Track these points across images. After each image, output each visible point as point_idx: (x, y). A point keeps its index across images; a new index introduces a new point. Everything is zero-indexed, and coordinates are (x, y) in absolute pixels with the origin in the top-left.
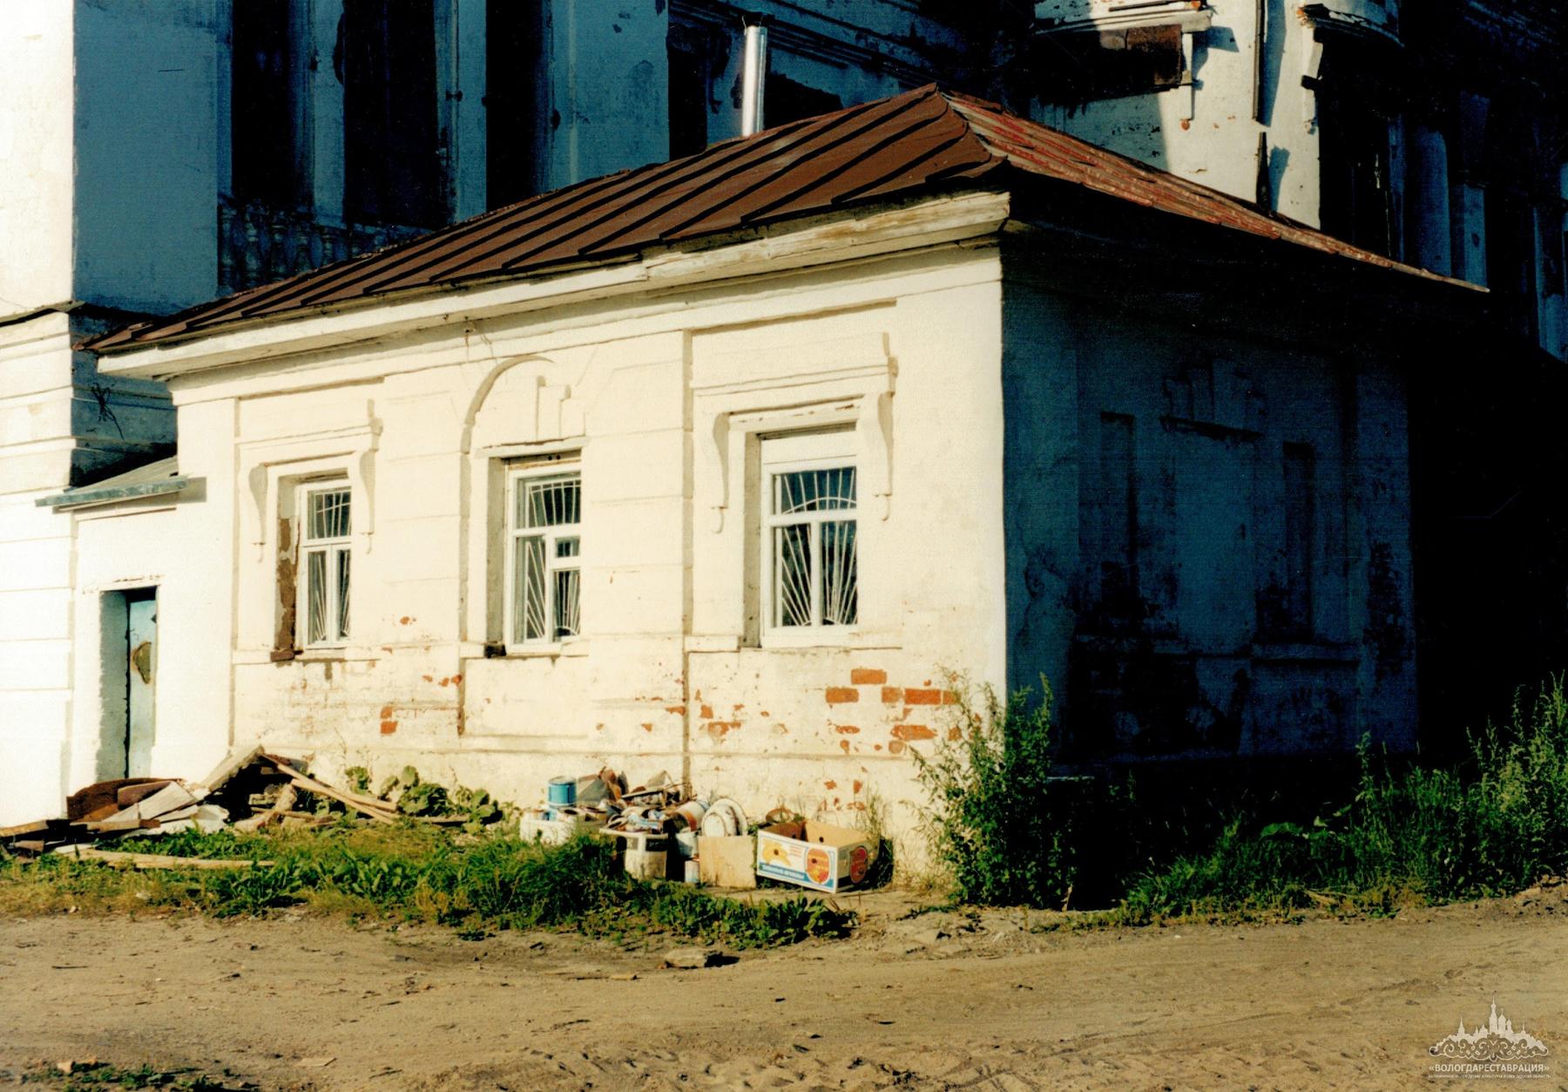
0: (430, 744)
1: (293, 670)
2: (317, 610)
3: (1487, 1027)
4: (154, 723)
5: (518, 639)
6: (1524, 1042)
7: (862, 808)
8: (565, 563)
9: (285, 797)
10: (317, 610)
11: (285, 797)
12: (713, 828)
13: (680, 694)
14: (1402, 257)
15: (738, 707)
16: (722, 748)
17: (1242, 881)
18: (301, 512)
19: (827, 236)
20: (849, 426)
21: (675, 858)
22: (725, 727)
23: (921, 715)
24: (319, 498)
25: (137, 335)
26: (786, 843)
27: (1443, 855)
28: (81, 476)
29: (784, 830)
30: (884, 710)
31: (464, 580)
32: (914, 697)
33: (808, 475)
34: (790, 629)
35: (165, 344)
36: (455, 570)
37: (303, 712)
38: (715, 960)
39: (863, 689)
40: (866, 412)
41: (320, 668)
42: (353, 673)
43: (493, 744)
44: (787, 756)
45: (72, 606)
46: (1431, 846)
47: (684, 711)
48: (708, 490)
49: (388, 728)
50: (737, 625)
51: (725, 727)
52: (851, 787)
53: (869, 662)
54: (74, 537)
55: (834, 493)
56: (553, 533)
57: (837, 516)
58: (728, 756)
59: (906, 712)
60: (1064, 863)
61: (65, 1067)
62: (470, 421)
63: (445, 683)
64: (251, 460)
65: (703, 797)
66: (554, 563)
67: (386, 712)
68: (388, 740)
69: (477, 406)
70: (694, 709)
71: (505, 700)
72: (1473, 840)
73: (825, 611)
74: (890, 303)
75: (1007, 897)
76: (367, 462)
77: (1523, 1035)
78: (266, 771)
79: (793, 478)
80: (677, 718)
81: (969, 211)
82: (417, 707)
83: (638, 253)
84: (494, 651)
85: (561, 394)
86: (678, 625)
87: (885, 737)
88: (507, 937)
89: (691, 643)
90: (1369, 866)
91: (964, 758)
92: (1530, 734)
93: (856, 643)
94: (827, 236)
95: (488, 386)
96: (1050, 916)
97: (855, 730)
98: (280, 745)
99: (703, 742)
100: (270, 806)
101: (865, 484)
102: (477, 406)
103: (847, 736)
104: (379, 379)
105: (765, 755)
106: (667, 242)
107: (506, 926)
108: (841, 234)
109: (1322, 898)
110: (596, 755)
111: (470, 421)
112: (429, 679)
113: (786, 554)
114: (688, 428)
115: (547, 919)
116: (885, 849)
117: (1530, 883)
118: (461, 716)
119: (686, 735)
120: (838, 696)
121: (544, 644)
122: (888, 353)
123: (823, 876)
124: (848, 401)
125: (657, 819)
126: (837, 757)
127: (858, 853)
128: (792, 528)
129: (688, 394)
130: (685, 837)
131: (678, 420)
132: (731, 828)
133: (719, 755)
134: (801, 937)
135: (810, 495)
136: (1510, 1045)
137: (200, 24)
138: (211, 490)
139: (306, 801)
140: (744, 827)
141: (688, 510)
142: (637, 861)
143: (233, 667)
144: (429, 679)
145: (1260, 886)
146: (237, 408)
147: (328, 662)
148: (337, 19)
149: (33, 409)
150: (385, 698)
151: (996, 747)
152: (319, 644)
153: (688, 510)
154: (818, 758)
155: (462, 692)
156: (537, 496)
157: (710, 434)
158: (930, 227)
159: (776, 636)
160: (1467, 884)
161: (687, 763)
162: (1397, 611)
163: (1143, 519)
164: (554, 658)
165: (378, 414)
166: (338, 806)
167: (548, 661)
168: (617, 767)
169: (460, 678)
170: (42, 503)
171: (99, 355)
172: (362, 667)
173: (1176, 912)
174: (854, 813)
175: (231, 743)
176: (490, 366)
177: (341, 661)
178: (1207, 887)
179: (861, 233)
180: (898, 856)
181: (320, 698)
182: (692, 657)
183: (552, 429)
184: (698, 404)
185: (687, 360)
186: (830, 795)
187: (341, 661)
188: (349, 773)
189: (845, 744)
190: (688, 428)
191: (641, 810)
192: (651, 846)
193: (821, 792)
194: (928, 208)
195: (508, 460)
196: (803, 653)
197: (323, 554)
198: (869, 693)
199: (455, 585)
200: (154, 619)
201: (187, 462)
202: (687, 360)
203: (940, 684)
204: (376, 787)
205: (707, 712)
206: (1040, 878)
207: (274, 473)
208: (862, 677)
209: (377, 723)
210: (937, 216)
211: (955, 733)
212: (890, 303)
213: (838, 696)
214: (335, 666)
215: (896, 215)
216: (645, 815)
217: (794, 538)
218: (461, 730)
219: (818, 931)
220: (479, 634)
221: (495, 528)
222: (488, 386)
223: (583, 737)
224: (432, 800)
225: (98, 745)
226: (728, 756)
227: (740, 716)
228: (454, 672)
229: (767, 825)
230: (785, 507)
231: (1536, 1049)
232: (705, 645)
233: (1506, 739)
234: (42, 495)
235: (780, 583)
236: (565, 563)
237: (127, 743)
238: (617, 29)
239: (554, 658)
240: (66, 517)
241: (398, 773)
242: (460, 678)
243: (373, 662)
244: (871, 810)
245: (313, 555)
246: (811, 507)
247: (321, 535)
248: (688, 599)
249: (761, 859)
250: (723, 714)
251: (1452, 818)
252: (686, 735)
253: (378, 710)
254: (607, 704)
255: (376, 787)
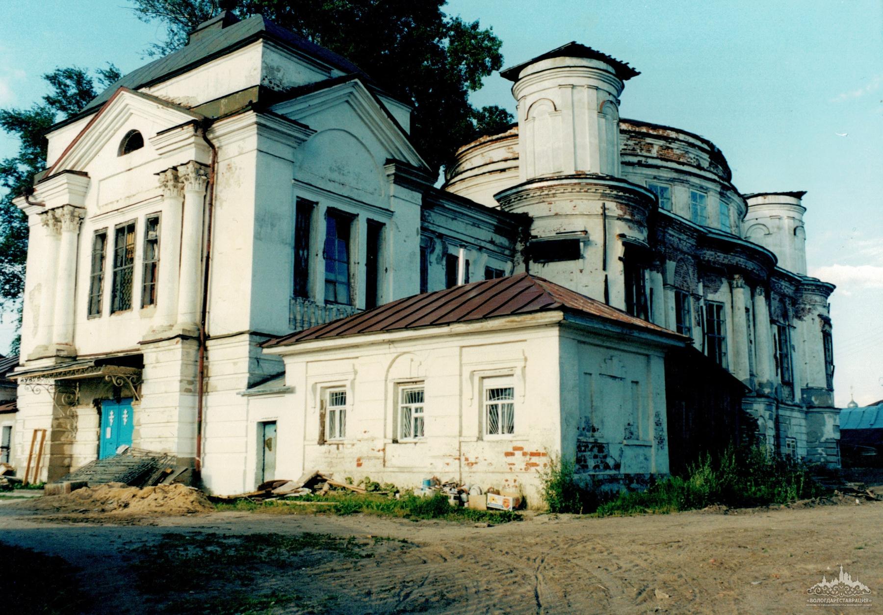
0: (373, 470)
1: (325, 448)
2: (332, 428)
3: (839, 580)
4: (275, 463)
5: (402, 438)
6: (858, 586)
7: (516, 487)
8: (419, 415)
9: (326, 487)
10: (332, 428)
11: (326, 487)
12: (473, 493)
13: (458, 454)
14: (635, 314)
15: (477, 458)
16: (471, 470)
17: (628, 506)
18: (328, 398)
19: (508, 322)
20: (512, 375)
21: (461, 503)
22: (472, 464)
23: (535, 460)
24: (333, 394)
25: (278, 343)
26: (496, 497)
27: (681, 499)
28: (251, 386)
29: (493, 492)
30: (523, 458)
31: (385, 419)
32: (532, 454)
33: (497, 390)
34: (491, 435)
35: (286, 345)
36: (383, 417)
37: (329, 460)
38: (489, 526)
39: (516, 452)
40: (518, 372)
41: (336, 446)
42: (346, 448)
43: (395, 470)
44: (493, 472)
45: (247, 427)
46: (678, 496)
47: (459, 459)
48: (467, 394)
49: (359, 465)
50: (477, 435)
51: (472, 464)
52: (513, 481)
53: (519, 444)
54: (248, 404)
55: (502, 395)
56: (414, 406)
57: (506, 402)
58: (474, 472)
59: (530, 459)
60: (580, 501)
61: (370, 536)
62: (388, 371)
63: (379, 451)
64: (311, 382)
65: (467, 484)
66: (414, 415)
67: (359, 460)
68: (359, 469)
69: (390, 366)
70: (463, 458)
71: (399, 456)
72: (689, 495)
73: (503, 430)
74: (525, 341)
75: (562, 511)
76: (353, 383)
77: (857, 583)
78: (319, 478)
79: (493, 391)
80: (457, 461)
81: (551, 317)
82: (369, 458)
83: (448, 324)
84: (395, 441)
85: (419, 364)
86: (458, 434)
87: (523, 466)
88: (425, 521)
89: (462, 439)
90: (661, 503)
91: (549, 471)
92: (704, 465)
93: (515, 439)
94: (508, 322)
95: (394, 361)
96: (577, 516)
97: (514, 464)
98: (324, 471)
99: (466, 468)
100: (321, 489)
101: (516, 393)
102: (390, 366)
103: (512, 466)
104: (357, 358)
105: (486, 472)
106: (458, 321)
107: (423, 518)
108: (512, 321)
109: (650, 511)
110: (430, 473)
111: (388, 371)
112: (373, 450)
113: (491, 413)
114: (461, 375)
115: (434, 517)
116: (524, 499)
117: (705, 507)
118: (384, 461)
119: (460, 466)
120: (508, 454)
121: (411, 439)
122: (524, 355)
123: (508, 506)
124: (512, 368)
125: (455, 491)
126: (508, 473)
127: (517, 500)
128: (492, 406)
129: (461, 365)
130: (464, 496)
131: (458, 373)
132: (479, 493)
133: (471, 472)
134: (509, 521)
135: (498, 396)
136: (850, 588)
137: (286, 244)
138: (297, 390)
139: (333, 487)
140: (483, 492)
141: (461, 399)
142: (452, 502)
143: (304, 446)
144: (373, 450)
145: (633, 507)
146: (307, 366)
147: (338, 445)
148: (324, 240)
149: (235, 364)
150: (358, 456)
151: (559, 468)
152: (332, 439)
153: (461, 399)
154: (502, 473)
155: (384, 453)
156: (408, 394)
157: (468, 376)
158: (540, 321)
159: (488, 437)
160: (688, 507)
161: (461, 474)
162: (662, 430)
163: (594, 404)
164: (415, 443)
165: (356, 368)
166: (344, 488)
167: (413, 445)
168: (438, 476)
169: (384, 450)
170: (238, 394)
171: (263, 348)
172: (349, 446)
173: (611, 514)
174: (514, 489)
175: (304, 470)
176: (396, 355)
177: (343, 444)
178: (618, 508)
179: (519, 322)
180: (528, 501)
181: (335, 455)
182: (462, 444)
183: (415, 375)
184: (464, 368)
185: (461, 355)
186: (506, 484)
187: (343, 444)
188: (346, 479)
189: (511, 469)
190: (461, 375)
191: (449, 488)
192: (455, 498)
193: (504, 483)
194: (539, 315)
195: (399, 383)
196: (497, 442)
197: (334, 411)
198: (518, 454)
199: (383, 421)
200: (275, 431)
201: (289, 380)
202: (461, 355)
203: (542, 451)
204: (355, 483)
205: (467, 459)
206: (574, 504)
207: (319, 386)
208: (516, 449)
209: (355, 463)
210: (542, 318)
211: (545, 465)
212: (525, 341)
213: (508, 454)
214: (341, 446)
215: (529, 316)
216: (451, 490)
217: (493, 408)
218: (384, 465)
219: (514, 519)
220: (390, 436)
221: (395, 403)
222: (394, 361)
223: (425, 467)
224: (376, 487)
225: (255, 471)
226: (474, 472)
227: (477, 461)
228: (382, 447)
229: (488, 492)
230: (490, 398)
231: (864, 590)
232: (466, 439)
233: (697, 467)
234: (238, 391)
235: (489, 422)
236: (419, 415)
237: (263, 470)
238: (405, 241)
239: (415, 443)
240: (245, 398)
241: (363, 479)
242: (384, 450)
243: (353, 445)
244: (520, 488)
245: (331, 411)
246: (498, 399)
247: (333, 405)
248: (461, 426)
249: (488, 502)
250: (472, 460)
251: (683, 489)
252: (460, 466)
253: (356, 459)
254: (434, 457)
255: (355, 483)
